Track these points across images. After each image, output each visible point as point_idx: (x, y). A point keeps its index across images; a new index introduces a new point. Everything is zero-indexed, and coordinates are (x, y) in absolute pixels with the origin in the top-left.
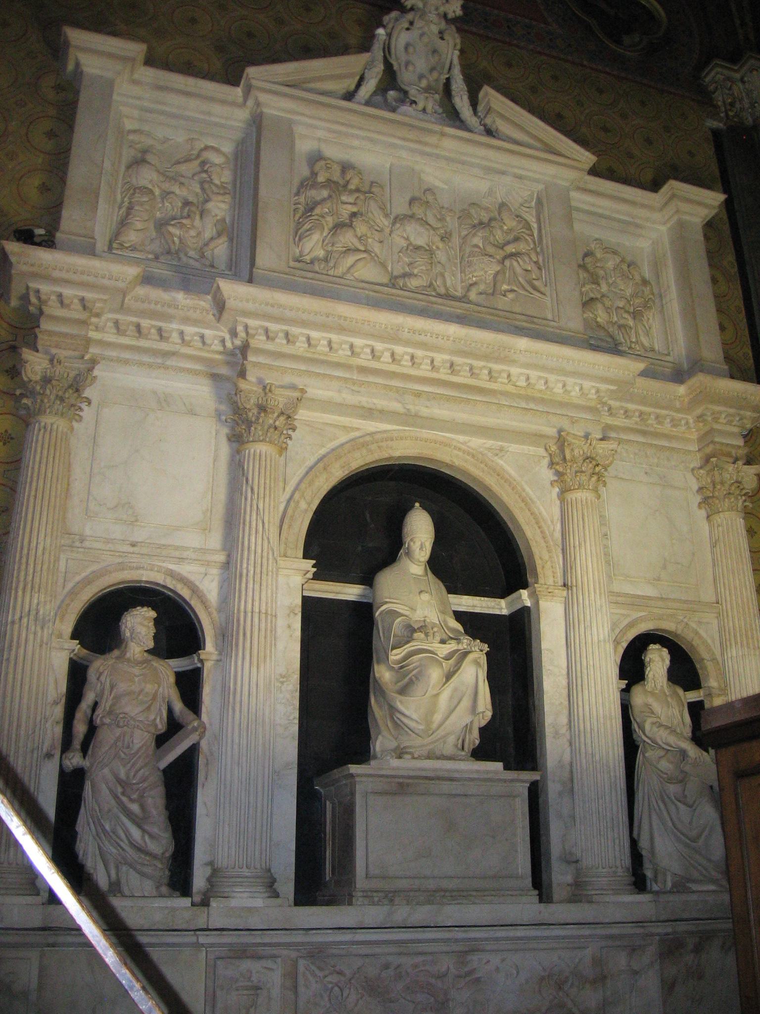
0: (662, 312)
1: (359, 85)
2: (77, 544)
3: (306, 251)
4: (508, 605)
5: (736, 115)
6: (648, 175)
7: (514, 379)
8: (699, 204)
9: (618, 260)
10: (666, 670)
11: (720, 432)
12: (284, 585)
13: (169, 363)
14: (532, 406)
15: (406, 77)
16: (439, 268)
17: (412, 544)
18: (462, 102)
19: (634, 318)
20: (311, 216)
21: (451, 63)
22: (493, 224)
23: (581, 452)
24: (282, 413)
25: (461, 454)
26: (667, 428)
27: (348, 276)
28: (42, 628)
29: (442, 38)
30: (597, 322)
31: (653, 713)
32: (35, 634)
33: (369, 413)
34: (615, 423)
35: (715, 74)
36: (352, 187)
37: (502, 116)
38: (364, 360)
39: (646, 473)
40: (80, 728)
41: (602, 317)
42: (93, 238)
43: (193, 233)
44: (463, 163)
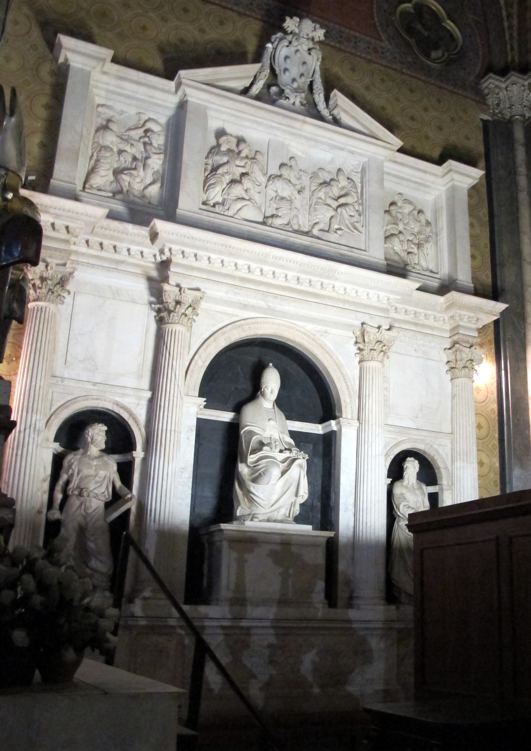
0: (436, 244)
1: (252, 84)
2: (60, 383)
3: (211, 198)
4: (323, 428)
5: (501, 112)
6: (436, 154)
7: (336, 289)
8: (468, 176)
9: (412, 208)
10: (416, 474)
11: (464, 327)
12: (186, 412)
13: (120, 268)
14: (347, 306)
15: (284, 79)
16: (295, 212)
17: (266, 389)
18: (319, 98)
19: (418, 248)
20: (215, 174)
21: (314, 70)
22: (333, 183)
23: (375, 338)
24: (190, 306)
25: (300, 334)
26: (430, 322)
27: (236, 216)
28: (38, 435)
29: (310, 54)
30: (394, 250)
31: (405, 499)
32: (34, 439)
33: (245, 307)
34: (399, 318)
35: (492, 82)
36: (243, 155)
37: (345, 111)
38: (244, 273)
39: (415, 350)
40: (59, 496)
41: (398, 247)
42: (75, 184)
43: (138, 180)
44: (316, 141)
